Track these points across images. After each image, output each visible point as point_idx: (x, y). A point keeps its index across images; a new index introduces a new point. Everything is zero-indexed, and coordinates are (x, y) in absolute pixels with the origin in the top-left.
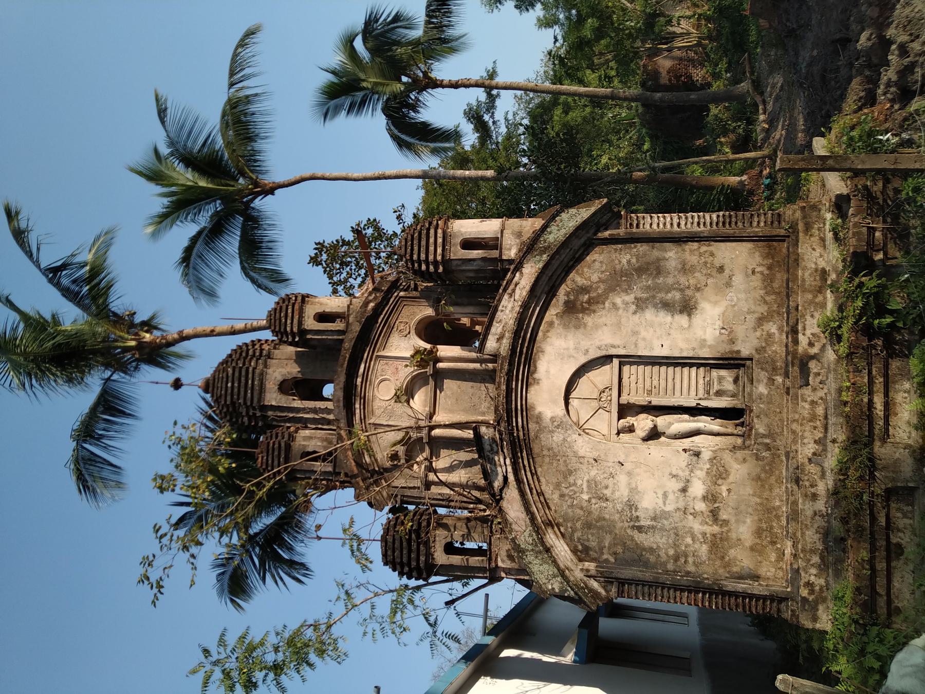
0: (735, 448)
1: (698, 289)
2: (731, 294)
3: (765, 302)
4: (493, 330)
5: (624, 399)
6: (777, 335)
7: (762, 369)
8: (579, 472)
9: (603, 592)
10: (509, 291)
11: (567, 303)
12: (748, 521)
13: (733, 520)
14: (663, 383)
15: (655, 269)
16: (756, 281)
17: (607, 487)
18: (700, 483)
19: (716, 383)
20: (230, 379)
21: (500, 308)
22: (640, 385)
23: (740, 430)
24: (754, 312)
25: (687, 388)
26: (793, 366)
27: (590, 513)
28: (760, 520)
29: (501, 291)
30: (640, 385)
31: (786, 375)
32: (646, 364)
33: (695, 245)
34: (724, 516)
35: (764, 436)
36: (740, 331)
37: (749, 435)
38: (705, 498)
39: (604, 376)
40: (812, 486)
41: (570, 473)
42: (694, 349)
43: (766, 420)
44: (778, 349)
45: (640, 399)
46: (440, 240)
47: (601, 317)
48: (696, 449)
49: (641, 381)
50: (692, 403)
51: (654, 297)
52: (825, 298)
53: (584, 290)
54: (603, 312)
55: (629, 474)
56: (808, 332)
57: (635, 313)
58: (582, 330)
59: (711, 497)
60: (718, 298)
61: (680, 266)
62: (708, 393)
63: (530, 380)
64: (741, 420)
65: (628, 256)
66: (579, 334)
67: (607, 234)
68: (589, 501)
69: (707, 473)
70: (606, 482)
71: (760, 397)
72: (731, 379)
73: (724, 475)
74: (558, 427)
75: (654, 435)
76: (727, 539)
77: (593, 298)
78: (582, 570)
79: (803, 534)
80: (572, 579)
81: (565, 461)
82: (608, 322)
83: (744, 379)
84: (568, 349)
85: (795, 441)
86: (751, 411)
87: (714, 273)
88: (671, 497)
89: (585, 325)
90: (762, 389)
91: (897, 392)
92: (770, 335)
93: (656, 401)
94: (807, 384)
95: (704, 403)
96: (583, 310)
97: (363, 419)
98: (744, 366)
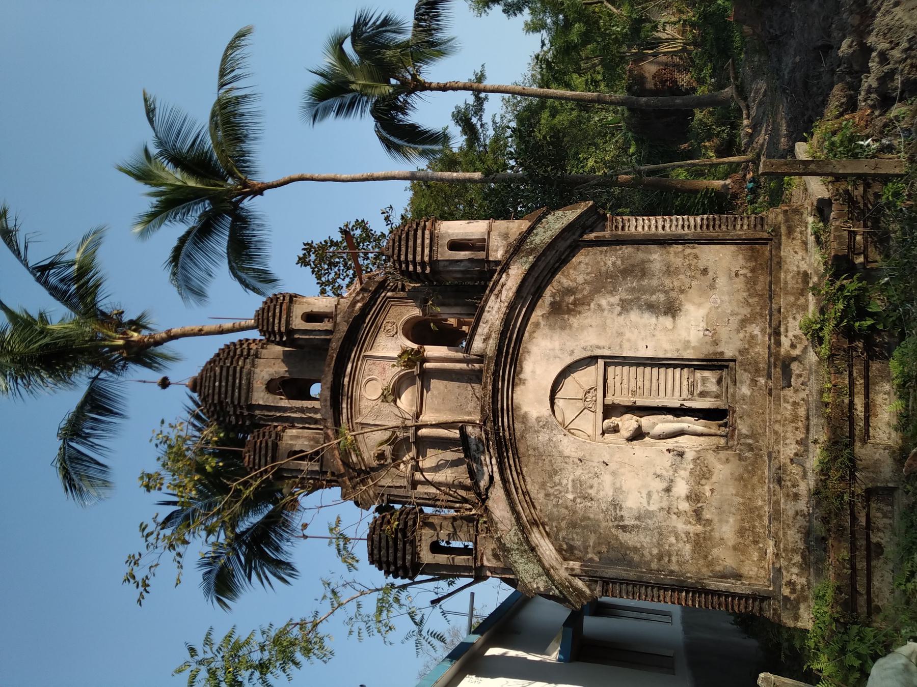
0: (718, 449)
1: (682, 291)
2: (715, 297)
3: (749, 304)
4: (480, 330)
5: (609, 400)
6: (760, 336)
7: (745, 370)
8: (564, 472)
9: (588, 591)
10: (496, 292)
11: (553, 304)
12: (731, 520)
13: (716, 519)
14: (647, 383)
15: (640, 271)
16: (740, 283)
17: (591, 487)
18: (684, 482)
19: (699, 385)
20: (218, 378)
21: (487, 309)
22: (625, 386)
23: (723, 431)
24: (737, 314)
25: (671, 389)
26: (775, 367)
27: (575, 512)
28: (743, 520)
29: (487, 292)
30: (625, 386)
31: (769, 376)
32: (631, 365)
33: (680, 248)
34: (707, 515)
35: (747, 437)
36: (724, 332)
37: (732, 436)
38: (688, 498)
39: (589, 376)
40: (794, 486)
41: (555, 472)
42: (678, 350)
43: (748, 421)
44: (760, 351)
45: (624, 399)
46: (427, 241)
47: (586, 318)
48: (680, 449)
49: (625, 381)
50: (675, 403)
51: (639, 299)
52: (807, 301)
53: (570, 291)
54: (589, 314)
55: (614, 474)
56: (790, 334)
57: (620, 314)
58: (567, 331)
59: (694, 497)
60: (702, 300)
61: (664, 268)
62: (692, 394)
63: (516, 380)
64: (724, 421)
65: (614, 259)
66: (565, 334)
67: (592, 236)
68: (574, 500)
69: (691, 473)
70: (591, 482)
71: (743, 398)
72: (714, 381)
73: (707, 476)
74: (543, 427)
75: (638, 435)
76: (710, 538)
77: (578, 300)
78: (567, 569)
79: (785, 534)
80: (557, 578)
81: (551, 461)
82: (594, 324)
83: (727, 380)
84: (553, 350)
85: (777, 442)
86: (734, 412)
87: (698, 275)
88: (655, 496)
89: (571, 326)
90: (745, 390)
91: (877, 393)
92: (753, 337)
93: (640, 402)
94: (790, 386)
95: (688, 404)
96: (569, 312)
97: (350, 419)
98: (727, 367)
